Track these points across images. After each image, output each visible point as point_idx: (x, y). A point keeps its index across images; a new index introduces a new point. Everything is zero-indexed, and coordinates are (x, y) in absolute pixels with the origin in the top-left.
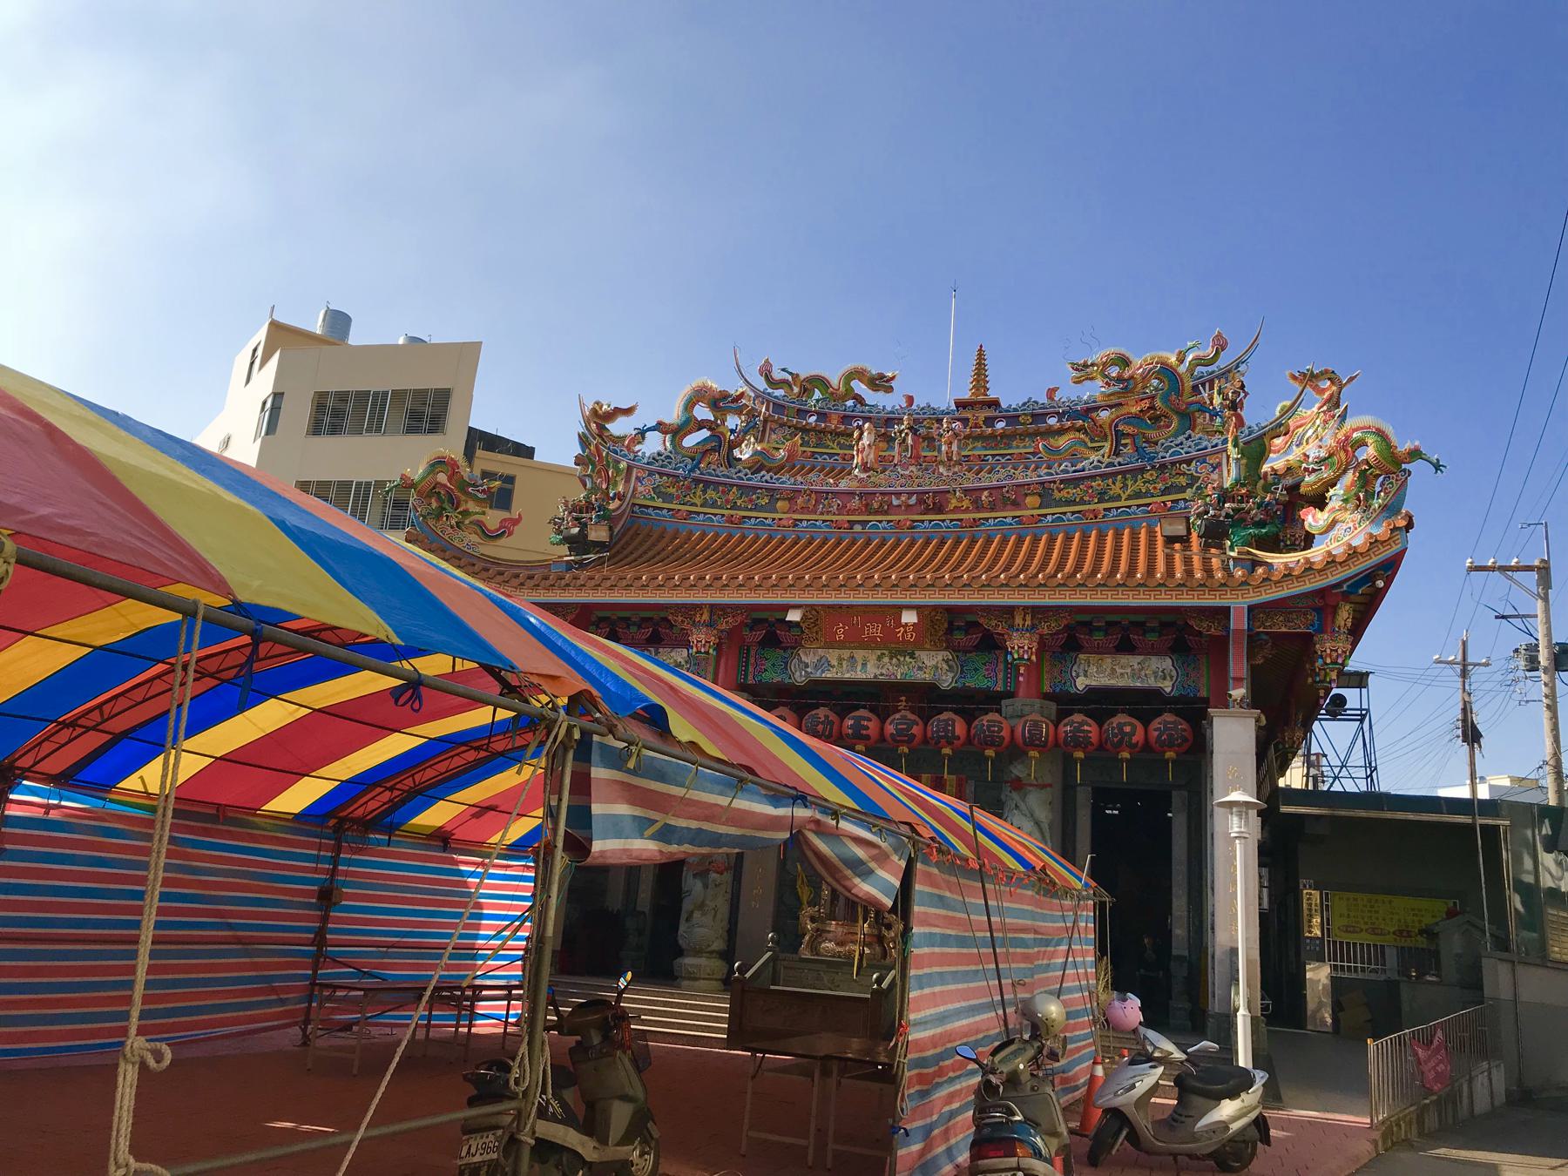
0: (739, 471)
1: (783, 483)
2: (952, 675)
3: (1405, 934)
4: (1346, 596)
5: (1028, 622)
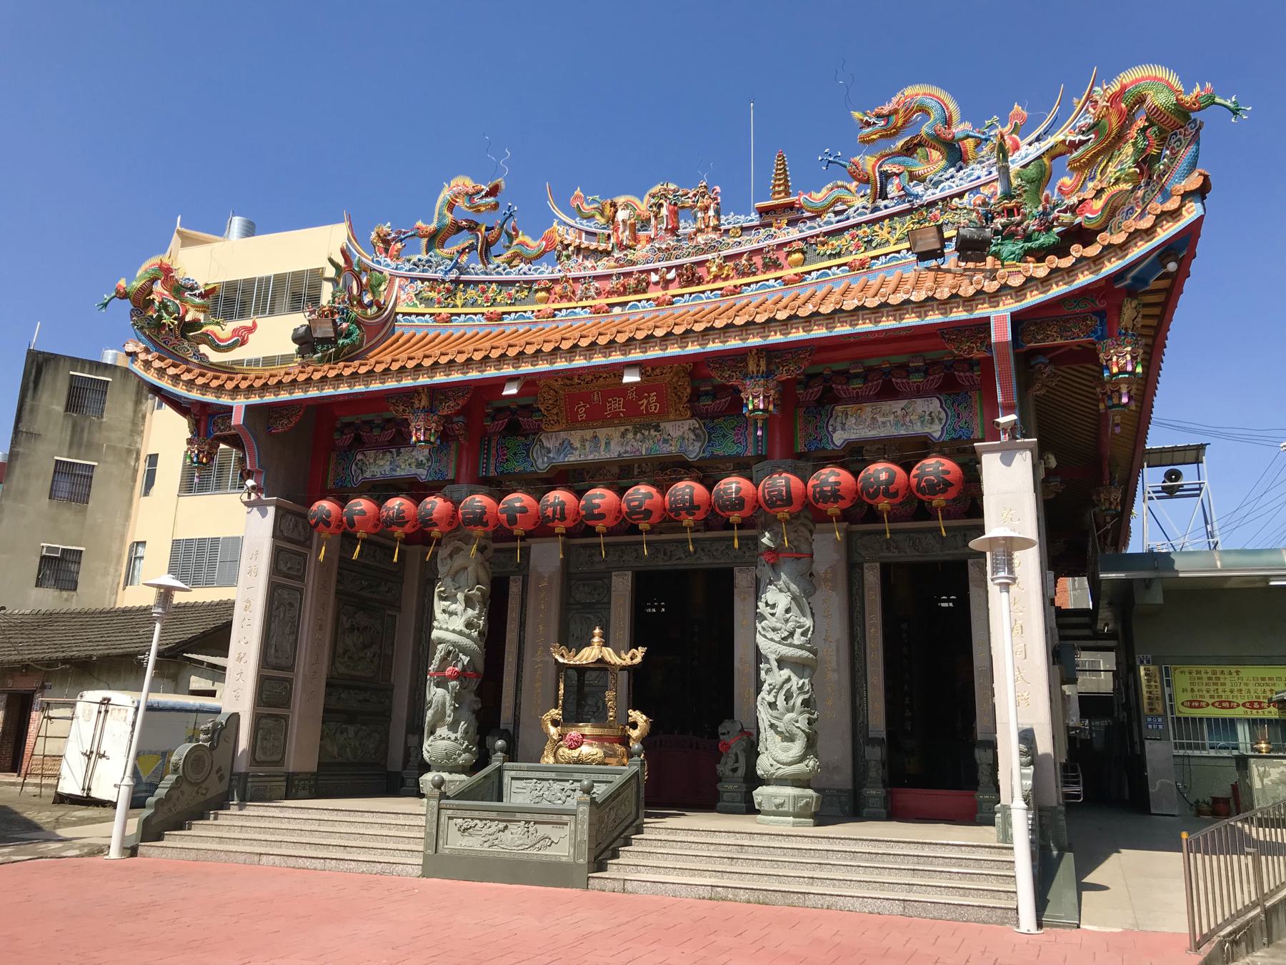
0: (498, 267)
1: (542, 273)
2: (700, 444)
3: (1256, 705)
4: (1131, 292)
5: (763, 367)
